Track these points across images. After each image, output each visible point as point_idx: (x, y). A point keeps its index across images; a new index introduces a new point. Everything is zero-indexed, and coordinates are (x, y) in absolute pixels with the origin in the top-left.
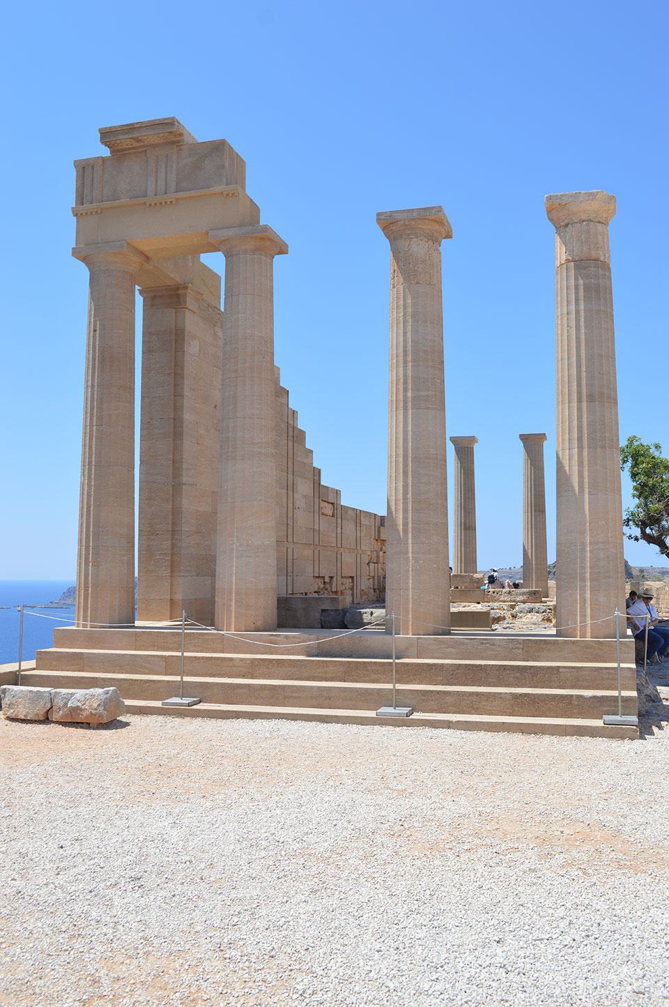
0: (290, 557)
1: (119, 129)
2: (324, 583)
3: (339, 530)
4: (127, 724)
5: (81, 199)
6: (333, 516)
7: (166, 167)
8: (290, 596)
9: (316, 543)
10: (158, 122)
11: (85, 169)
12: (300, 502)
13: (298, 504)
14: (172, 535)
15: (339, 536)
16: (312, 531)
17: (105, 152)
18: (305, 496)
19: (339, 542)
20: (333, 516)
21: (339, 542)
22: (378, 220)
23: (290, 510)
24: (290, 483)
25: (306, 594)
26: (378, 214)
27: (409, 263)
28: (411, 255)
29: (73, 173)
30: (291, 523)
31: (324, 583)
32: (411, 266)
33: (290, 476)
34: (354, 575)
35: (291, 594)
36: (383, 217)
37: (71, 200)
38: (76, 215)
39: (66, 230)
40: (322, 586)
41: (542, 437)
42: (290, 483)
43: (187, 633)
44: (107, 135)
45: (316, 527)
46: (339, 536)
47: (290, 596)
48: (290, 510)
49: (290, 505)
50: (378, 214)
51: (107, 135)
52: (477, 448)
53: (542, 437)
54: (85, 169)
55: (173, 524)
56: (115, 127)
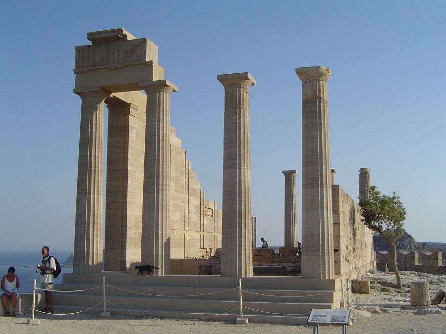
0: (186, 238)
2: (207, 252)
3: (216, 224)
5: (78, 66)
6: (212, 216)
7: (119, 51)
9: (202, 230)
11: (80, 50)
12: (192, 209)
13: (191, 210)
15: (216, 226)
17: (90, 43)
19: (216, 230)
20: (212, 216)
21: (216, 230)
22: (218, 79)
23: (187, 214)
24: (187, 199)
26: (218, 76)
29: (75, 51)
31: (207, 252)
33: (187, 196)
37: (73, 65)
38: (75, 73)
39: (71, 80)
40: (205, 254)
41: (294, 172)
42: (187, 199)
43: (34, 282)
44: (90, 36)
45: (202, 222)
46: (216, 226)
48: (187, 214)
49: (187, 211)
50: (218, 76)
51: (90, 36)
53: (294, 172)
54: (80, 50)
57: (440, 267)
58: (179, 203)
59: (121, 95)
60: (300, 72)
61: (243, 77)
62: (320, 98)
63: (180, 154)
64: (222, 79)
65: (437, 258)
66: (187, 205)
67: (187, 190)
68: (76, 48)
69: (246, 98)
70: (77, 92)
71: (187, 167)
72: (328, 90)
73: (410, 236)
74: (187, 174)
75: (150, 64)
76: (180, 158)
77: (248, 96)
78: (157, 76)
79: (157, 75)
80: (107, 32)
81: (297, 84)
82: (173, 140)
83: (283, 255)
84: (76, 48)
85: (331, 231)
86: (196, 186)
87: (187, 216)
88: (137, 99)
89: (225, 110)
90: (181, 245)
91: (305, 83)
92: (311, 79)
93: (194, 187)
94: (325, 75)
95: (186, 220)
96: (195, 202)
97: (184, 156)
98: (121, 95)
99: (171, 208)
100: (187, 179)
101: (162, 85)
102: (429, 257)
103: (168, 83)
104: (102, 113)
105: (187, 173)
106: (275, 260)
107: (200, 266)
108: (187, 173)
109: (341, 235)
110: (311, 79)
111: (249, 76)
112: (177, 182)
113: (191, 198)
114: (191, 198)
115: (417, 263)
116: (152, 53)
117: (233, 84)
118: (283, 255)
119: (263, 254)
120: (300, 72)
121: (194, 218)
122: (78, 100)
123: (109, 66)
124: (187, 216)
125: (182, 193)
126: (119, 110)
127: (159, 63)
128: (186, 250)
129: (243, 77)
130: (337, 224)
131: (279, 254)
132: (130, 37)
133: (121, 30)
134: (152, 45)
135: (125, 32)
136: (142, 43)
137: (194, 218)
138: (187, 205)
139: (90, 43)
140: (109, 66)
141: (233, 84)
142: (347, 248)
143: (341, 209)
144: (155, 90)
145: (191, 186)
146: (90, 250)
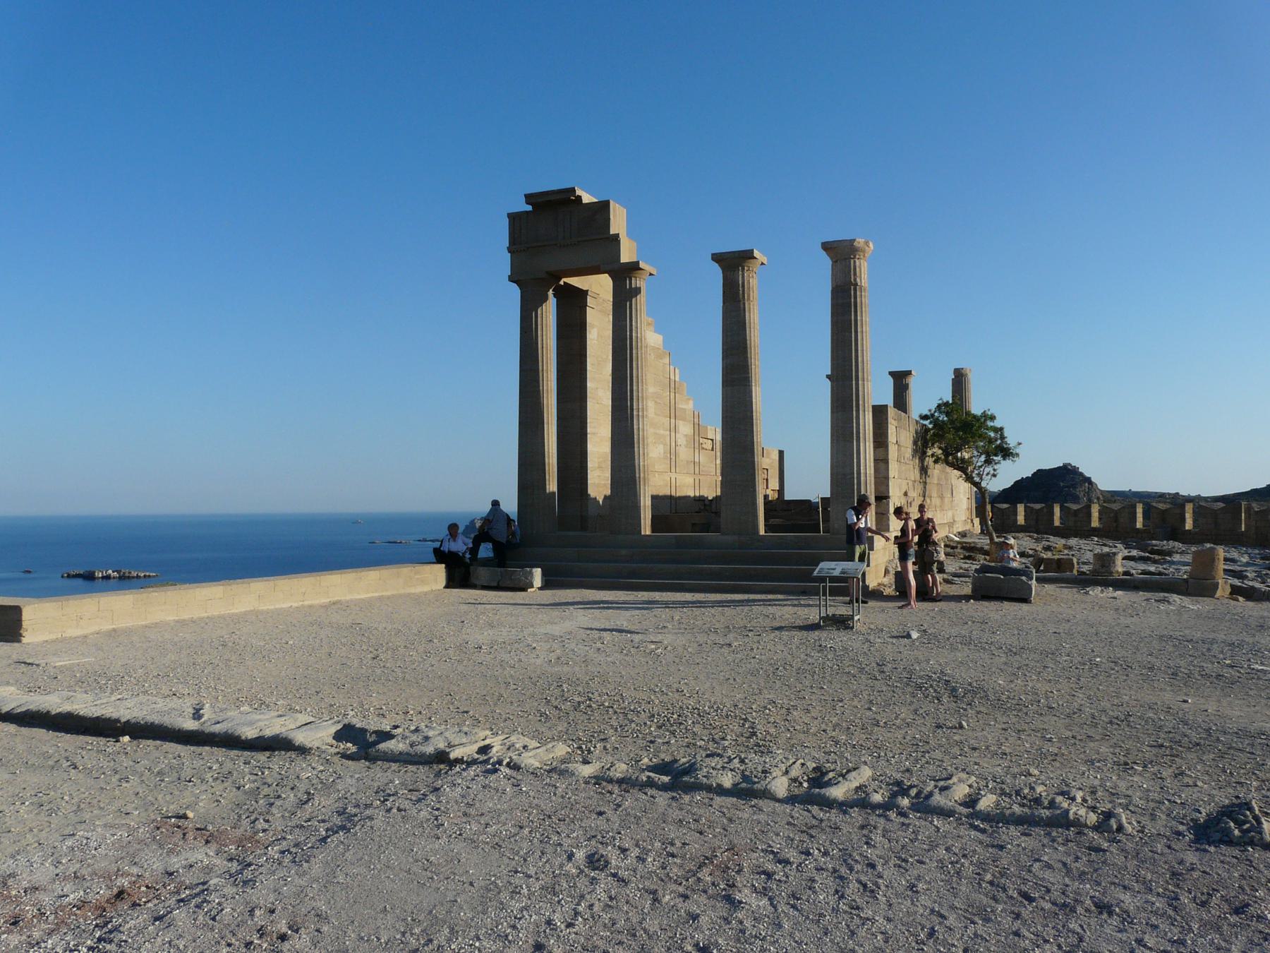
11: (514, 218)
12: (682, 441)
17: (529, 208)
37: (506, 242)
39: (503, 262)
44: (529, 198)
51: (529, 198)
54: (514, 218)
57: (1095, 529)
59: (575, 281)
60: (827, 247)
61: (748, 255)
62: (856, 285)
64: (718, 258)
65: (1089, 515)
67: (674, 413)
68: (509, 215)
70: (511, 279)
72: (865, 272)
73: (1088, 480)
74: (673, 387)
77: (754, 281)
78: (626, 257)
79: (627, 254)
80: (553, 192)
81: (825, 263)
82: (649, 337)
84: (509, 215)
85: (871, 470)
86: (688, 406)
88: (599, 287)
91: (835, 262)
92: (842, 255)
94: (864, 252)
95: (672, 457)
96: (685, 429)
97: (667, 361)
98: (575, 281)
99: (650, 440)
101: (634, 267)
102: (1076, 512)
103: (642, 265)
104: (549, 312)
109: (891, 475)
110: (842, 255)
111: (756, 254)
113: (680, 424)
114: (680, 424)
115: (1057, 523)
116: (618, 222)
117: (733, 264)
120: (827, 247)
121: (684, 453)
122: (515, 291)
126: (573, 304)
127: (630, 234)
129: (748, 255)
130: (882, 462)
132: (587, 198)
133: (573, 190)
135: (579, 192)
136: (603, 207)
137: (684, 453)
139: (529, 208)
140: (557, 242)
141: (733, 264)
142: (906, 494)
143: (892, 438)
144: (624, 275)
146: (555, 439)
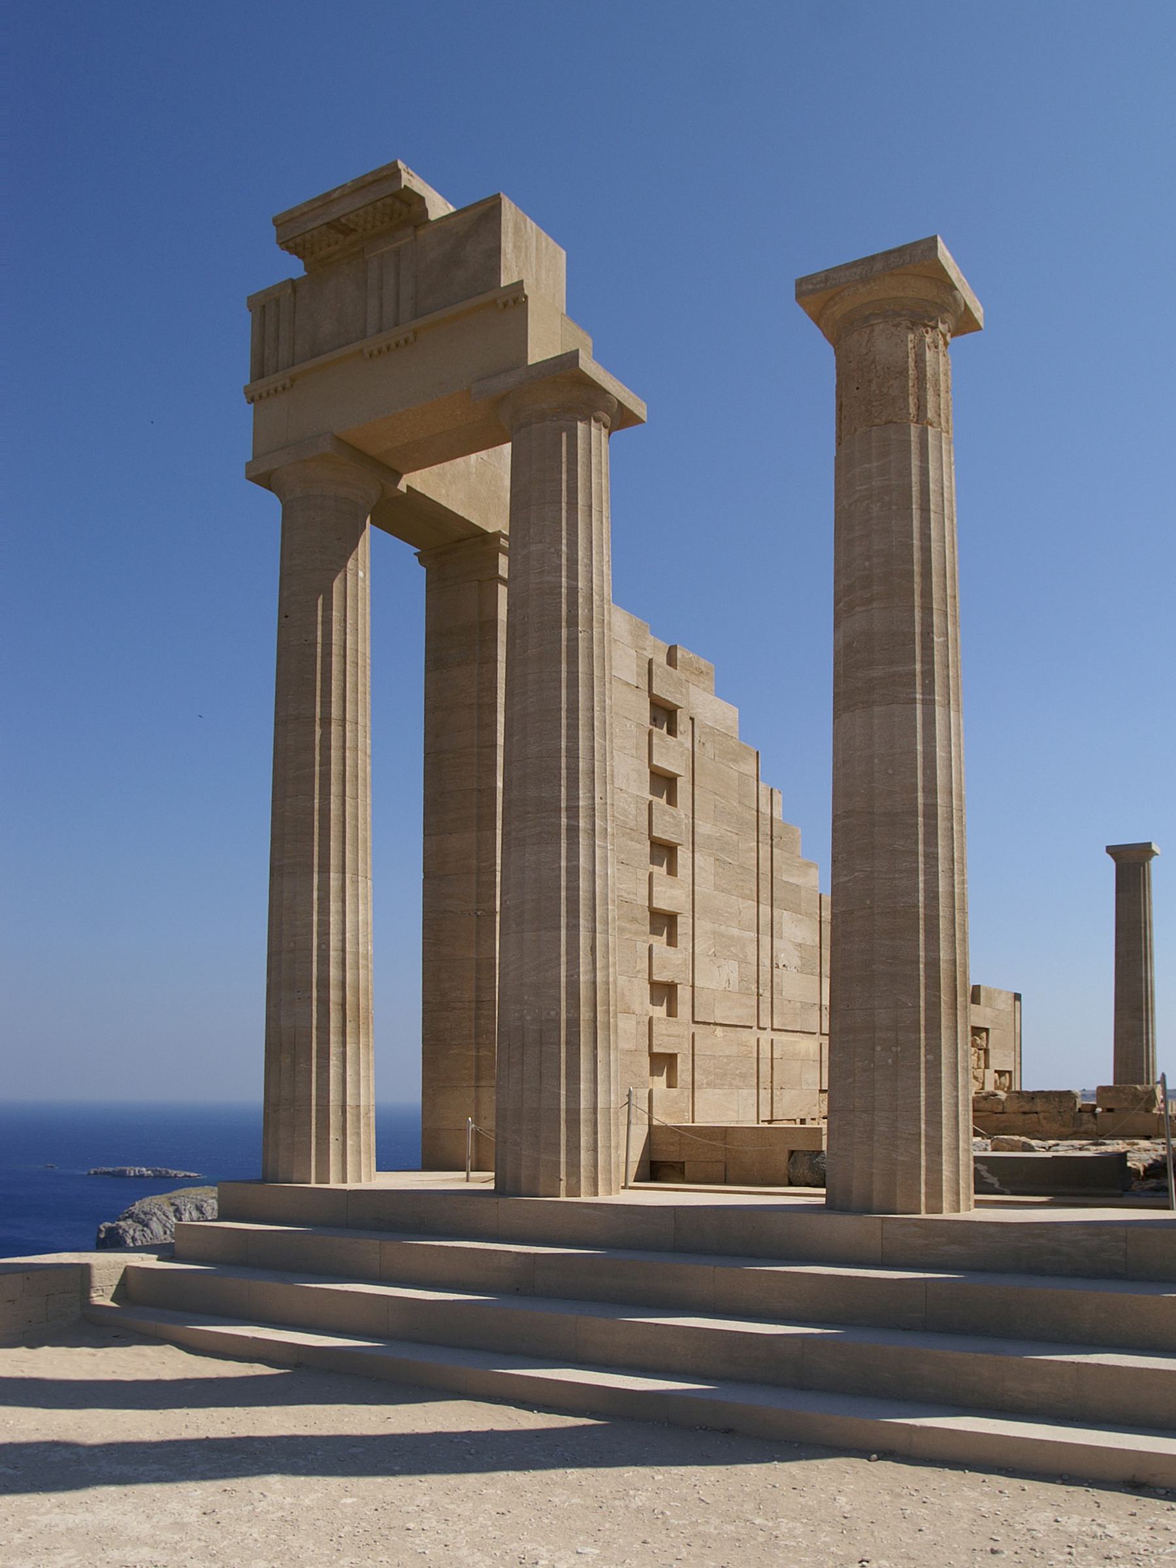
1: (306, 209)
4: (1163, 1076)
5: (260, 370)
8: (766, 1125)
10: (370, 179)
12: (787, 955)
13: (782, 959)
14: (477, 1008)
16: (817, 1008)
17: (295, 268)
18: (800, 945)
25: (803, 1121)
27: (870, 381)
28: (873, 362)
29: (247, 317)
30: (767, 994)
32: (874, 387)
33: (765, 909)
34: (1011, 1069)
35: (770, 1122)
36: (811, 287)
38: (252, 400)
44: (293, 233)
47: (766, 1125)
49: (766, 961)
51: (293, 233)
52: (1155, 866)
55: (478, 988)
56: (298, 208)
58: (735, 932)
63: (735, 761)
66: (765, 940)
69: (936, 374)
71: (765, 808)
75: (516, 298)
76: (736, 774)
83: (1110, 1110)
87: (765, 977)
89: (839, 444)
90: (743, 1076)
93: (791, 880)
97: (750, 768)
100: (765, 850)
105: (765, 828)
106: (1082, 1129)
107: (792, 1152)
108: (765, 828)
112: (722, 856)
116: (532, 259)
118: (1110, 1110)
119: (1014, 1112)
122: (267, 508)
123: (374, 338)
124: (765, 977)
125: (700, 868)
128: (765, 1095)
131: (1094, 1107)
132: (438, 207)
134: (528, 225)
135: (411, 180)
136: (482, 220)
138: (765, 940)
145: (783, 876)
